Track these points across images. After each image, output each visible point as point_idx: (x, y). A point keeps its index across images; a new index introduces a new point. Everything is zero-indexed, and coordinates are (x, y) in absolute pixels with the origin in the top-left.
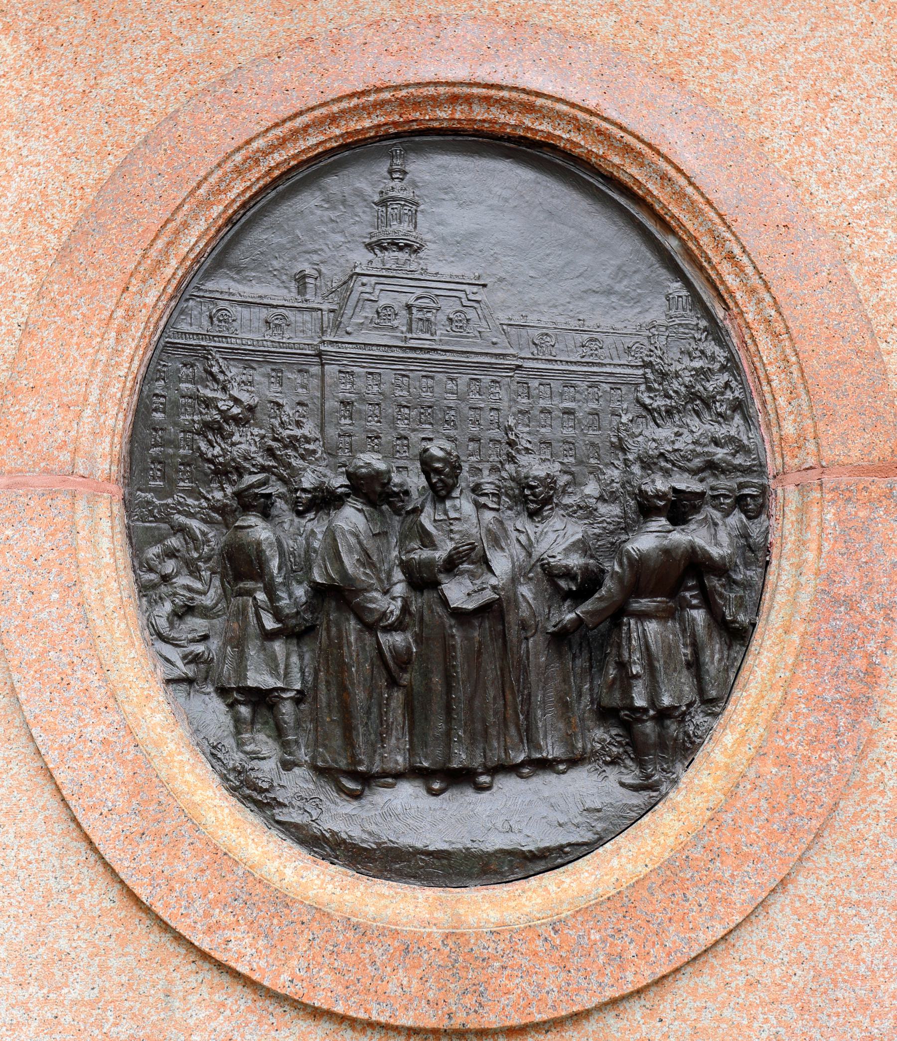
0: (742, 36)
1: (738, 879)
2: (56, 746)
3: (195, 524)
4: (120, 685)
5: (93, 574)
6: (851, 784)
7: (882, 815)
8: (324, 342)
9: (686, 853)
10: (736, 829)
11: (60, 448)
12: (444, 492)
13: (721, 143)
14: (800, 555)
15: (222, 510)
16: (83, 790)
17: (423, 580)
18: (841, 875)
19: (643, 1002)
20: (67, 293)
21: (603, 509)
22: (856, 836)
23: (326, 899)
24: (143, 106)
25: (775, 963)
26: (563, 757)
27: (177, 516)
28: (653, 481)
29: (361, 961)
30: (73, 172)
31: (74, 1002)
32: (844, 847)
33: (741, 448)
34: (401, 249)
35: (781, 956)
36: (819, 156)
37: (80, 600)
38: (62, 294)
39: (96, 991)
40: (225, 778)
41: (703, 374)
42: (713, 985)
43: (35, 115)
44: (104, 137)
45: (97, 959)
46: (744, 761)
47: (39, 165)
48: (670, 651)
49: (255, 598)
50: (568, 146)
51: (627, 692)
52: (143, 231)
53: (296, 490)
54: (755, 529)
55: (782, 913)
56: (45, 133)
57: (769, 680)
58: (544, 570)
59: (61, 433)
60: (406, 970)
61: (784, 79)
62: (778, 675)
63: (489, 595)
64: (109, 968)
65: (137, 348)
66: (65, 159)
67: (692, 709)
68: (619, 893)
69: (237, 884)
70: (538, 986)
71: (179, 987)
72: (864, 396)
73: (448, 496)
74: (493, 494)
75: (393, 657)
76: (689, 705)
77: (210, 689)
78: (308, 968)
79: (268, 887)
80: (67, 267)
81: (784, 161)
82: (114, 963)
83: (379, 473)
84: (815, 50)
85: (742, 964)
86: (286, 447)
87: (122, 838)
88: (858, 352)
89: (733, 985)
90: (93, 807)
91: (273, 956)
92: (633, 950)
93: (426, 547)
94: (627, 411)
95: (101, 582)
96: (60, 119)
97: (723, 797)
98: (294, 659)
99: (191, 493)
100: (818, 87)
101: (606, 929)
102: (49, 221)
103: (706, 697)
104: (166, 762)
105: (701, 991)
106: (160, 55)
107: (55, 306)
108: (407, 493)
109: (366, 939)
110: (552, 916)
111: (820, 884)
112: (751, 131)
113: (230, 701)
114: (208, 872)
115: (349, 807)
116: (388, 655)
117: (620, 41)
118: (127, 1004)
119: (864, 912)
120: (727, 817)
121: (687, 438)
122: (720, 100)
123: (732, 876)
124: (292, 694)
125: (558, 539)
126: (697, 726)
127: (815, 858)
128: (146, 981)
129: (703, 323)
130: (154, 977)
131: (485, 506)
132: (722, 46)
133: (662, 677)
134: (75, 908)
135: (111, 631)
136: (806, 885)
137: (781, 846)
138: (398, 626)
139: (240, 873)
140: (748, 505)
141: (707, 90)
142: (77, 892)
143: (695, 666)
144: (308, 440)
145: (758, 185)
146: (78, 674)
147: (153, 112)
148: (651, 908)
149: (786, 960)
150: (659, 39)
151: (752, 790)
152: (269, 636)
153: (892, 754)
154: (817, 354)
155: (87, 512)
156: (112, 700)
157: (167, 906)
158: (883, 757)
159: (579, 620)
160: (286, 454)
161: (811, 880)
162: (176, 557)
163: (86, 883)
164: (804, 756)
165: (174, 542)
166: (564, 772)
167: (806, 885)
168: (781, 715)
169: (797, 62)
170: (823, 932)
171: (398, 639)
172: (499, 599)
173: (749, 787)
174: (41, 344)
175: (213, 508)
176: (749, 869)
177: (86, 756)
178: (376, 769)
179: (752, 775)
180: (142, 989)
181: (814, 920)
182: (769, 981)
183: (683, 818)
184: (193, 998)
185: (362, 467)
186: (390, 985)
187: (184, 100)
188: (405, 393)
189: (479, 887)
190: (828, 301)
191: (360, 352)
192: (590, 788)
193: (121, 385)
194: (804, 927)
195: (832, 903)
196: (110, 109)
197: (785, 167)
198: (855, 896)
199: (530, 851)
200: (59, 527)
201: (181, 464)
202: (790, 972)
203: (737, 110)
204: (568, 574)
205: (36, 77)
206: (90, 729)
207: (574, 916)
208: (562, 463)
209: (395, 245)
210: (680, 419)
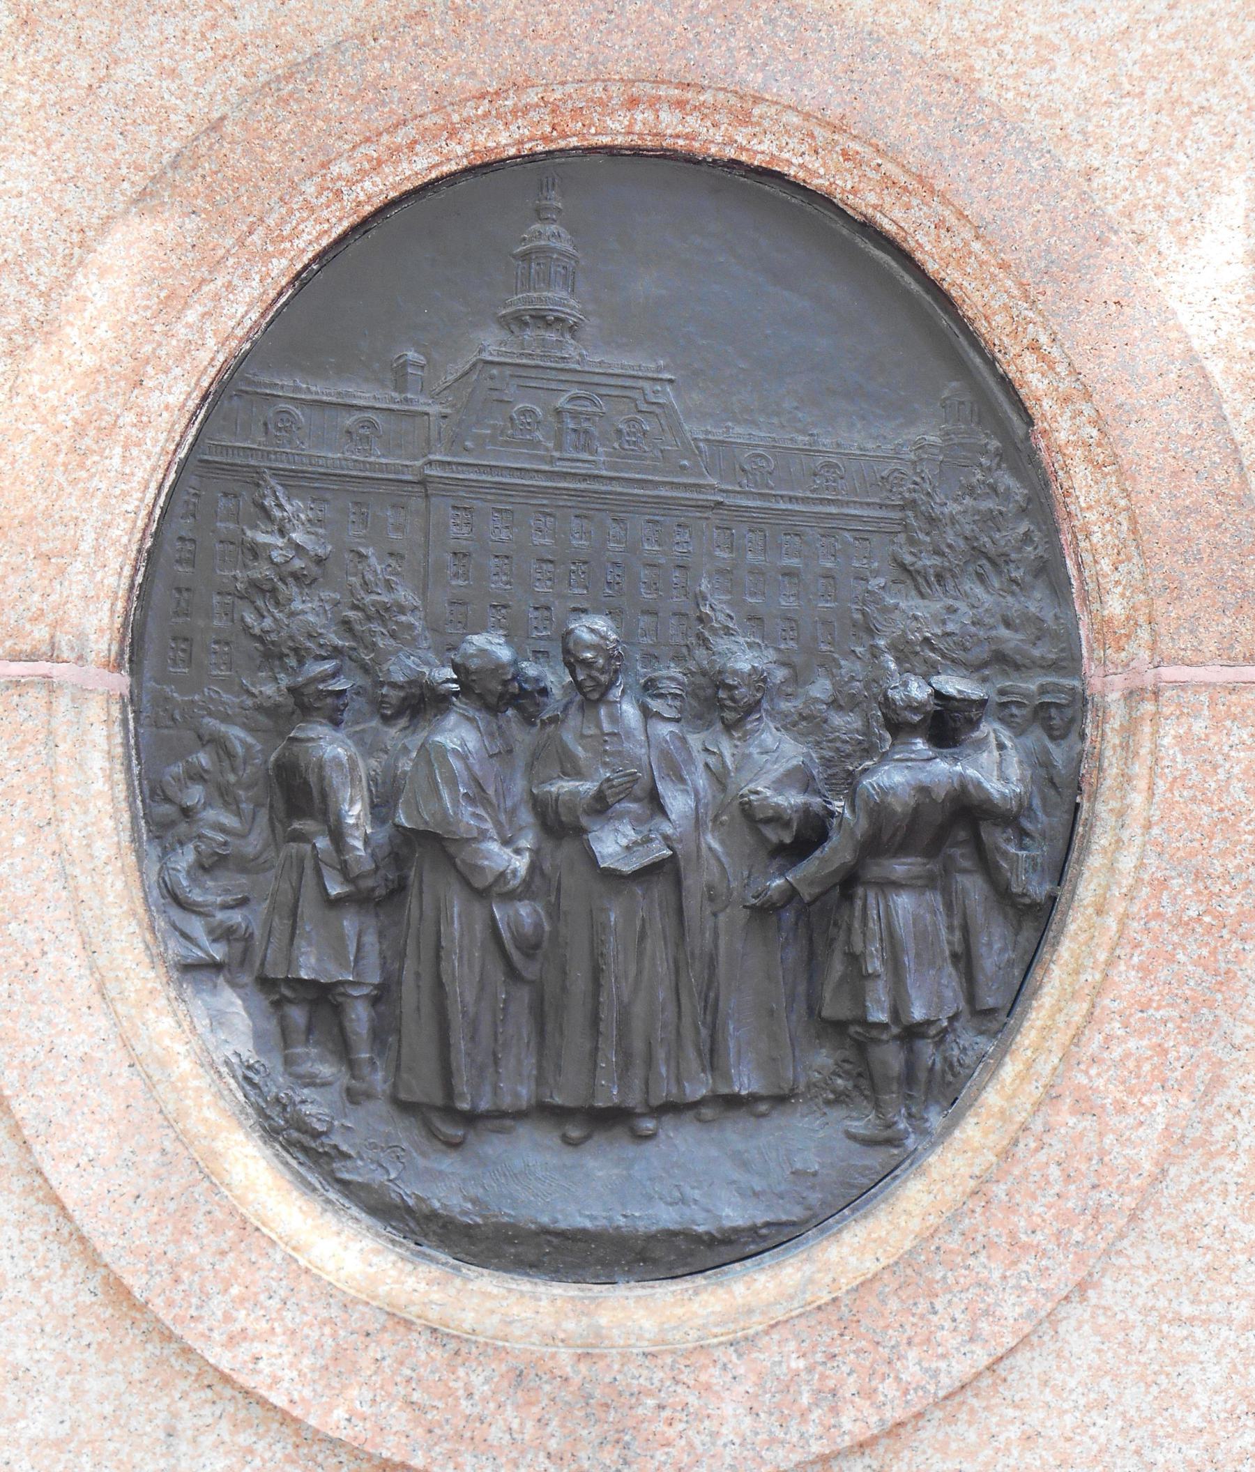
0: (1064, 15)
1: (1012, 1282)
2: (16, 1062)
3: (236, 734)
4: (111, 975)
5: (77, 808)
6: (1187, 1141)
7: (1232, 1188)
8: (430, 463)
9: (937, 1242)
10: (1012, 1209)
11: (34, 620)
12: (595, 696)
13: (1026, 177)
14: (1123, 798)
15: (272, 711)
16: (53, 1129)
17: (560, 826)
18: (1167, 1278)
19: (867, 1461)
20: (52, 387)
21: (837, 720)
22: (1191, 1220)
23: (403, 1300)
24: (175, 109)
25: (1066, 1406)
26: (763, 1092)
27: (207, 720)
28: (905, 684)
29: (451, 1393)
30: (70, 206)
31: (35, 1442)
32: (1173, 1236)
33: (1041, 633)
34: (549, 325)
35: (1074, 1397)
36: (1173, 197)
37: (56, 847)
38: (44, 389)
39: (67, 1425)
40: (261, 1112)
41: (991, 520)
42: (972, 1436)
43: (18, 121)
44: (117, 155)
45: (69, 1378)
46: (1028, 1107)
47: (20, 195)
48: (924, 937)
49: (314, 846)
50: (801, 175)
51: (859, 999)
52: (168, 297)
53: (382, 684)
54: (1058, 754)
55: (1078, 1335)
56: (31, 147)
57: (1071, 984)
58: (743, 810)
59: (36, 597)
60: (517, 1407)
61: (1124, 80)
62: (1083, 978)
63: (660, 851)
64: (85, 1392)
65: (154, 470)
66: (59, 187)
67: (957, 1024)
68: (835, 1300)
69: (274, 1274)
70: (711, 1434)
71: (186, 1423)
72: (1225, 561)
73: (603, 699)
74: (675, 696)
75: (514, 938)
76: (952, 1019)
77: (247, 979)
78: (374, 1401)
79: (319, 1279)
80: (54, 349)
81: (1120, 204)
82: (94, 1385)
83: (499, 667)
84: (1173, 37)
85: (1016, 1407)
86: (369, 618)
87: (107, 1203)
88: (1219, 495)
89: (1002, 1438)
90: (67, 1156)
91: (323, 1383)
92: (851, 1384)
93: (565, 774)
94: (877, 574)
95: (88, 819)
96: (53, 126)
97: (994, 1159)
98: (370, 939)
99: (226, 683)
100: (1174, 94)
101: (814, 1353)
102: (33, 279)
103: (978, 1008)
104: (175, 1089)
105: (954, 1446)
106: (203, 35)
107: (35, 408)
108: (544, 692)
109: (460, 1360)
110: (735, 1332)
111: (1136, 1290)
112: (1073, 157)
113: (277, 997)
114: (231, 1255)
115: (448, 1163)
116: (505, 935)
117: (883, 20)
118: (111, 1446)
119: (1199, 1333)
120: (999, 1190)
121: (965, 613)
122: (1028, 111)
123: (1004, 1277)
124: (365, 991)
125: (771, 765)
126: (964, 1050)
127: (1130, 1252)
128: (139, 1413)
129: (994, 444)
130: (152, 1407)
131: (658, 715)
132: (1035, 29)
133: (910, 979)
134: (39, 1302)
135: (101, 894)
136: (1115, 1291)
137: (1077, 1235)
138: (527, 890)
139: (278, 1257)
140: (1050, 718)
141: (1010, 95)
142: (41, 1279)
143: (965, 960)
144: (402, 610)
145: (1079, 240)
146: (51, 957)
147: (190, 119)
148: (882, 1323)
149: (1082, 1401)
150: (940, 17)
151: (1037, 1150)
152: (335, 903)
153: (1250, 1098)
154: (1158, 496)
155: (71, 716)
156: (98, 997)
157: (170, 1304)
158: (1237, 1102)
159: (791, 893)
160: (370, 630)
161: (1123, 1284)
162: (205, 781)
163: (56, 1266)
164: (1116, 1101)
165: (203, 759)
166: (763, 1115)
167: (1115, 1291)
168: (1084, 1039)
169: (1144, 55)
170: (1138, 1363)
171: (524, 910)
172: (674, 857)
173: (1033, 1145)
174: (12, 463)
175: (259, 708)
176: (1027, 1268)
177: (59, 1078)
178: (484, 1105)
179: (1037, 1126)
180: (133, 1424)
181: (1126, 1344)
182: (1055, 1434)
183: (935, 1188)
184: (208, 1440)
185: (472, 656)
186: (493, 1428)
187: (235, 100)
188: (547, 541)
189: (632, 1284)
190: (1176, 416)
191: (484, 477)
192: (812, 1139)
193: (128, 526)
194: (1110, 1354)
195: (1153, 1319)
196: (127, 113)
197: (1122, 214)
198: (1187, 1310)
199: (708, 1233)
200: (29, 737)
201: (216, 642)
202: (1087, 1420)
203: (1053, 126)
204: (777, 819)
205: (21, 63)
206: (64, 1039)
207: (767, 1333)
208: (778, 650)
209: (541, 319)
210: (956, 586)
